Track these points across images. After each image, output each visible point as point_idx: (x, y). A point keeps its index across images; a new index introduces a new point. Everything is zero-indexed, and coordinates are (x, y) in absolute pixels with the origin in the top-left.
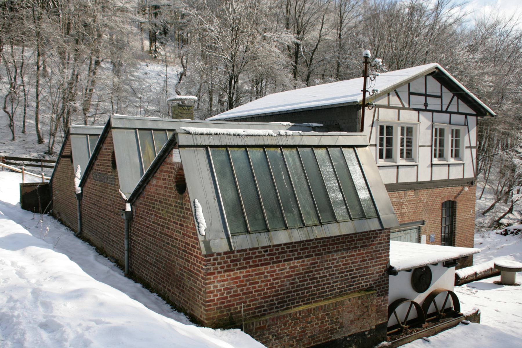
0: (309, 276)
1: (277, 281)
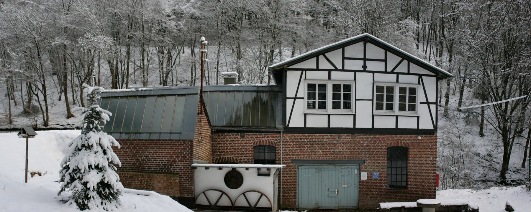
0: (134, 158)
1: (152, 163)
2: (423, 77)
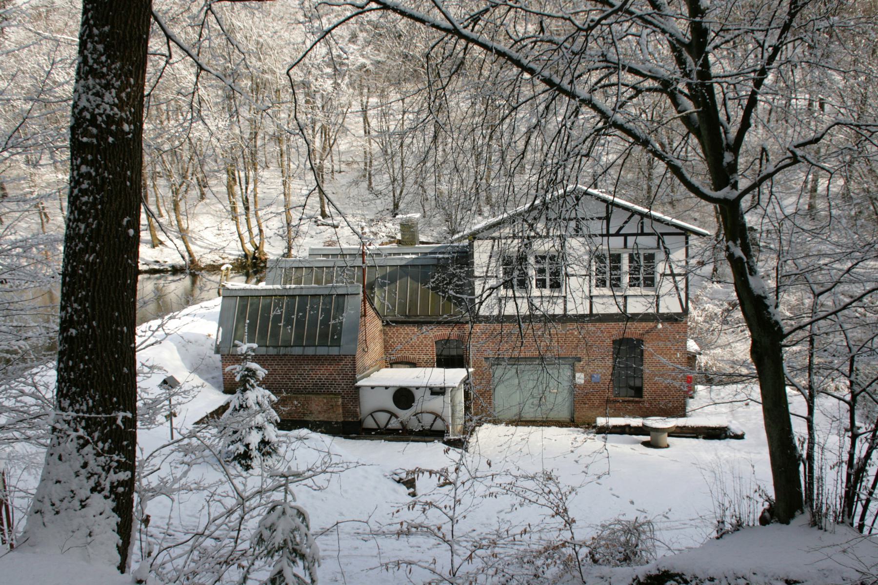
2: (666, 238)
